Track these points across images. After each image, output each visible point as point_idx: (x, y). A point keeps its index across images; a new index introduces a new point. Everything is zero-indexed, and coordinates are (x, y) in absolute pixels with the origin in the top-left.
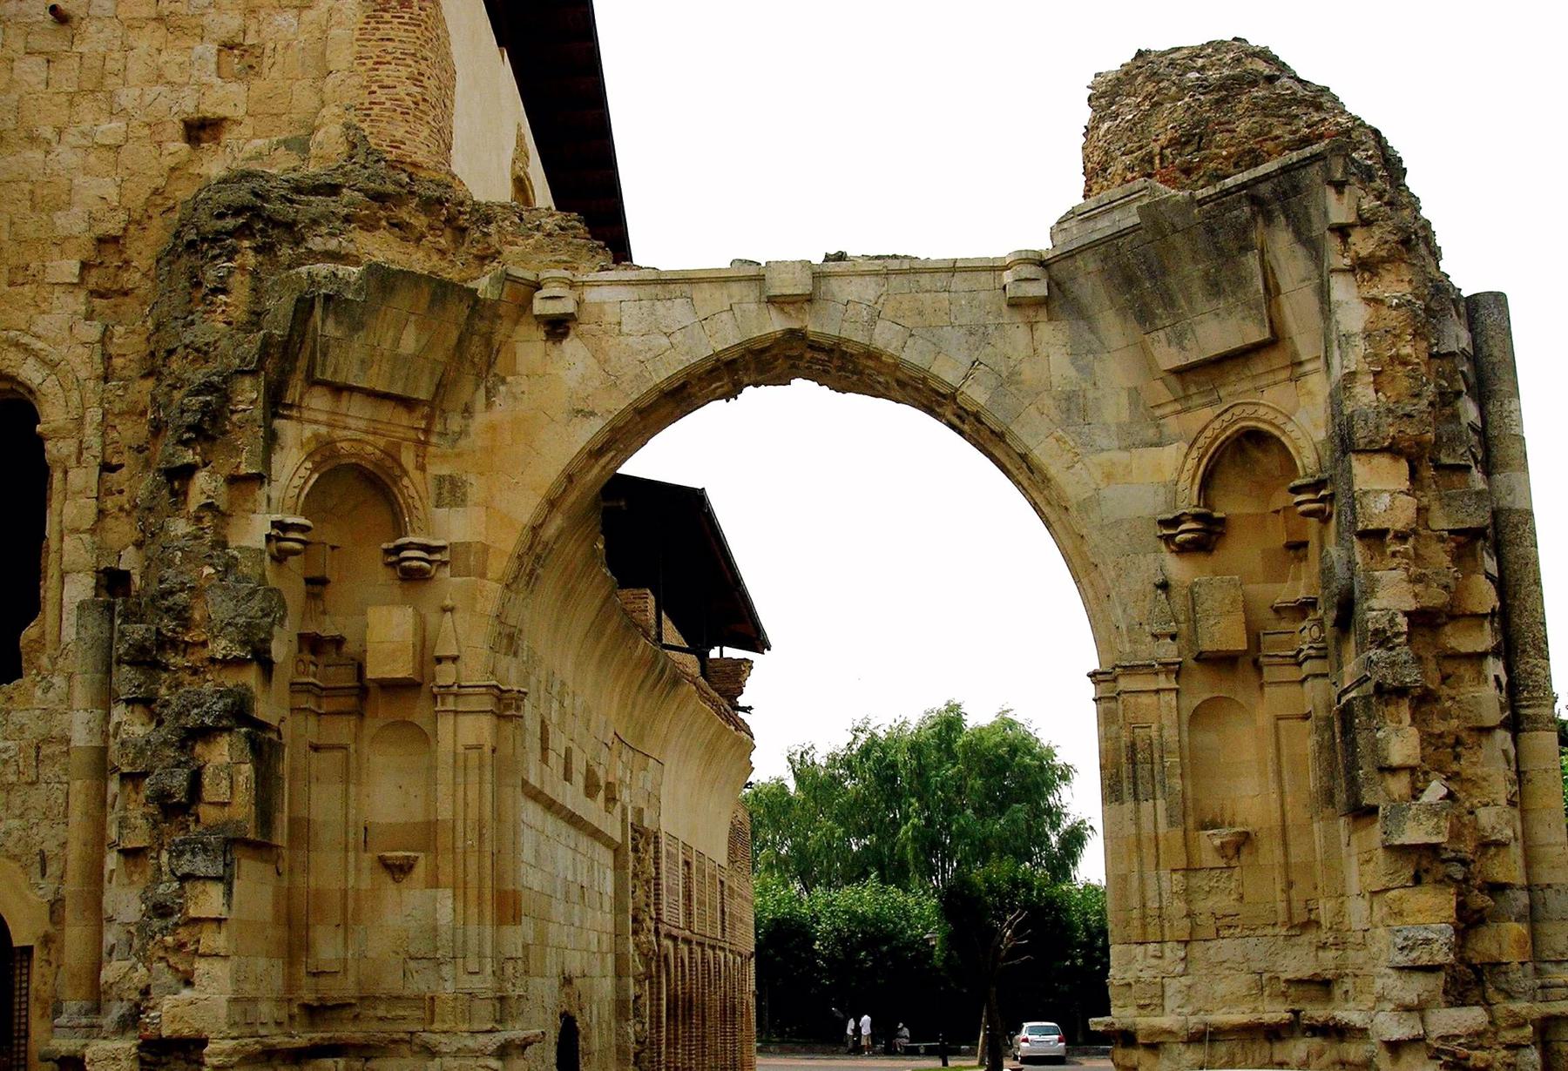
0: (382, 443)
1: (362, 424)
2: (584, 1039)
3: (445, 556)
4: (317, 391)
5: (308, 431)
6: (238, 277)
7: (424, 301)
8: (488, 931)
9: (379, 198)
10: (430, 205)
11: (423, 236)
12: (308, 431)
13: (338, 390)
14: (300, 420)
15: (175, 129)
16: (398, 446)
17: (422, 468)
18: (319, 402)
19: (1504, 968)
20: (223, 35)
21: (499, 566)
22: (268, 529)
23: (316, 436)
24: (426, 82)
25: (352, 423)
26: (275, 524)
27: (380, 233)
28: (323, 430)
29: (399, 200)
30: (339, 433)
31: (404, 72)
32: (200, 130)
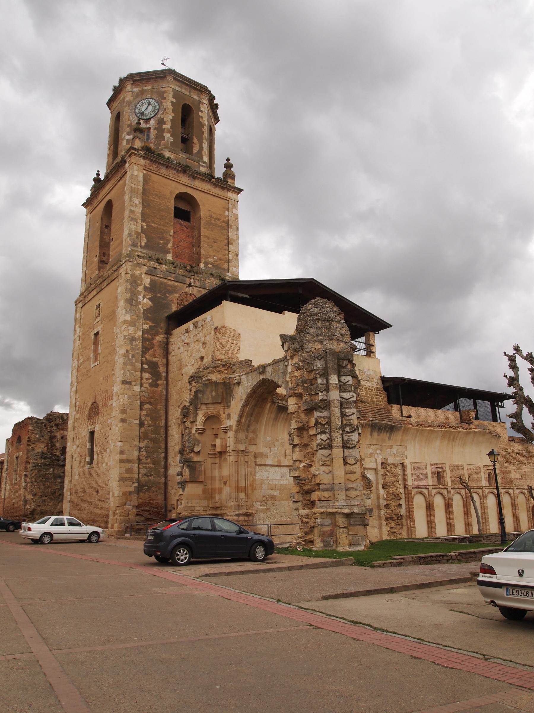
0: (216, 410)
1: (213, 408)
2: (363, 511)
3: (228, 428)
4: (203, 405)
5: (203, 411)
6: (193, 388)
7: (214, 387)
8: (236, 494)
9: (214, 368)
10: (224, 366)
11: (223, 372)
12: (203, 411)
13: (206, 404)
14: (201, 410)
15: (199, 360)
16: (220, 410)
17: (224, 413)
18: (204, 407)
19: (122, 514)
20: (202, 342)
21: (234, 428)
22: (195, 430)
23: (205, 412)
24: (223, 343)
25: (211, 408)
26: (196, 429)
27: (216, 374)
28: (206, 411)
29: (218, 367)
30: (209, 411)
31: (219, 343)
32: (202, 358)
